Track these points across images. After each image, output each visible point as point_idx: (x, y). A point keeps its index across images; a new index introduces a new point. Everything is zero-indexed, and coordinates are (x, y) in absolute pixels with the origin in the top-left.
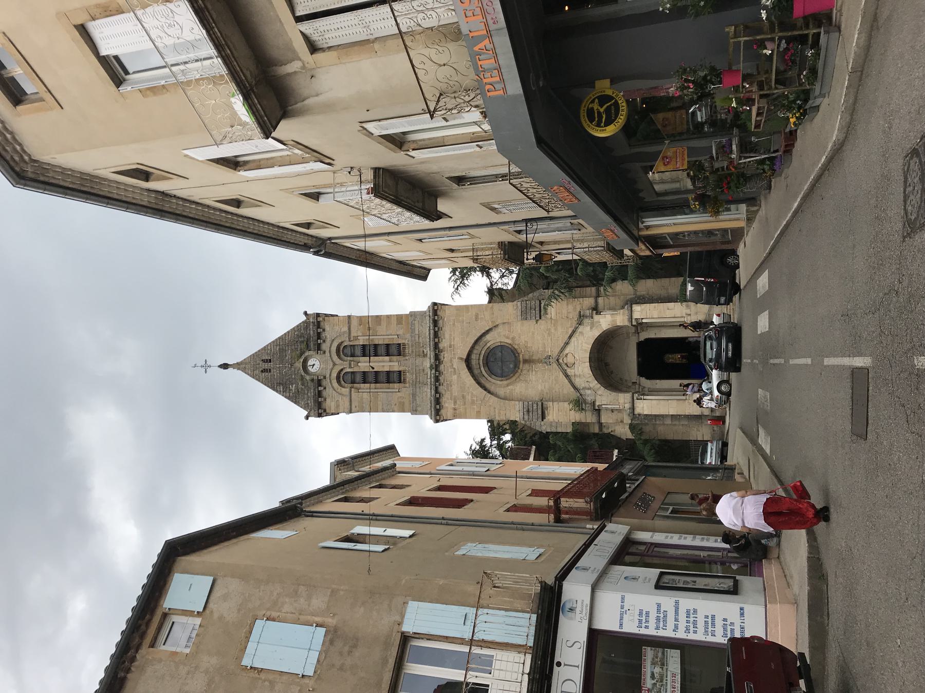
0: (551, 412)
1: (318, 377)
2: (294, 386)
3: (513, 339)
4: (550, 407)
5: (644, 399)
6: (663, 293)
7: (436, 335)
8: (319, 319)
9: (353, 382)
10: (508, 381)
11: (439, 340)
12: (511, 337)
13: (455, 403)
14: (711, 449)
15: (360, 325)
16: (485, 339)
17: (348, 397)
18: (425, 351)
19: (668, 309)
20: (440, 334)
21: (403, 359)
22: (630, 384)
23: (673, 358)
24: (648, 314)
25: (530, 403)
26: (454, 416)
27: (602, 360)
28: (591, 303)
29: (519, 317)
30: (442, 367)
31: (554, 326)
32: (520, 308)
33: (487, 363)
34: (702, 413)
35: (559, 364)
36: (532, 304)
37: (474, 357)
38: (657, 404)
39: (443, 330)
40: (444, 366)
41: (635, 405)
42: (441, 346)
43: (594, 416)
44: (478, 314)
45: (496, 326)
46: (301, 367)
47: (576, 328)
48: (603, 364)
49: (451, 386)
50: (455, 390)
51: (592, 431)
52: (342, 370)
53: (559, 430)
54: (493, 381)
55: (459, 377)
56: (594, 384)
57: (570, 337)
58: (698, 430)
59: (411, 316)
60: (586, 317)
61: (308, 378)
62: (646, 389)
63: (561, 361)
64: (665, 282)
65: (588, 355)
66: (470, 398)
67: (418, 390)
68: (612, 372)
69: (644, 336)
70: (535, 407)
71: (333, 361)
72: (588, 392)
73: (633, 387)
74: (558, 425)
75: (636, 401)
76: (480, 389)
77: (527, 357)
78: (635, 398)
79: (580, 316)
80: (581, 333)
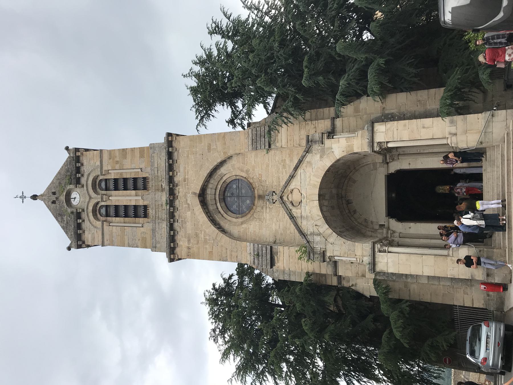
0: (281, 258)
1: (77, 210)
2: (66, 217)
3: (247, 171)
4: (280, 252)
5: (388, 252)
6: (420, 109)
7: (171, 168)
8: (78, 154)
9: (107, 215)
10: (244, 219)
11: (173, 174)
12: (245, 170)
13: (189, 241)
14: (488, 337)
15: (110, 159)
16: (220, 172)
17: (101, 230)
18: (163, 185)
19: (424, 127)
20: (175, 166)
21: (147, 193)
22: (377, 227)
23: (443, 189)
24: (395, 136)
25: (260, 246)
26: (188, 256)
27: (342, 197)
28: (327, 127)
29: (250, 147)
30: (177, 203)
31: (290, 156)
32: (251, 136)
33: (223, 199)
34: (472, 276)
35: (283, 203)
36: (262, 130)
37: (209, 191)
38: (407, 260)
39: (178, 162)
40: (179, 201)
41: (377, 260)
42: (176, 179)
43: (330, 266)
44: (210, 144)
45: (230, 157)
46: (64, 200)
47: (303, 157)
48: (344, 202)
49: (186, 223)
50: (189, 227)
51: (329, 283)
52: (98, 203)
53: (293, 279)
54: (229, 218)
55: (193, 213)
56: (325, 228)
57: (296, 168)
58: (465, 293)
59: (151, 148)
60: (315, 142)
61: (69, 210)
62: (397, 235)
63: (285, 198)
64: (423, 94)
65: (317, 191)
66: (202, 236)
67: (157, 225)
68: (355, 212)
69: (395, 167)
70: (264, 251)
71: (89, 195)
72: (317, 239)
73: (380, 231)
74: (292, 273)
75: (378, 254)
76: (213, 228)
77: (261, 193)
78: (376, 250)
79: (308, 141)
80: (309, 163)
